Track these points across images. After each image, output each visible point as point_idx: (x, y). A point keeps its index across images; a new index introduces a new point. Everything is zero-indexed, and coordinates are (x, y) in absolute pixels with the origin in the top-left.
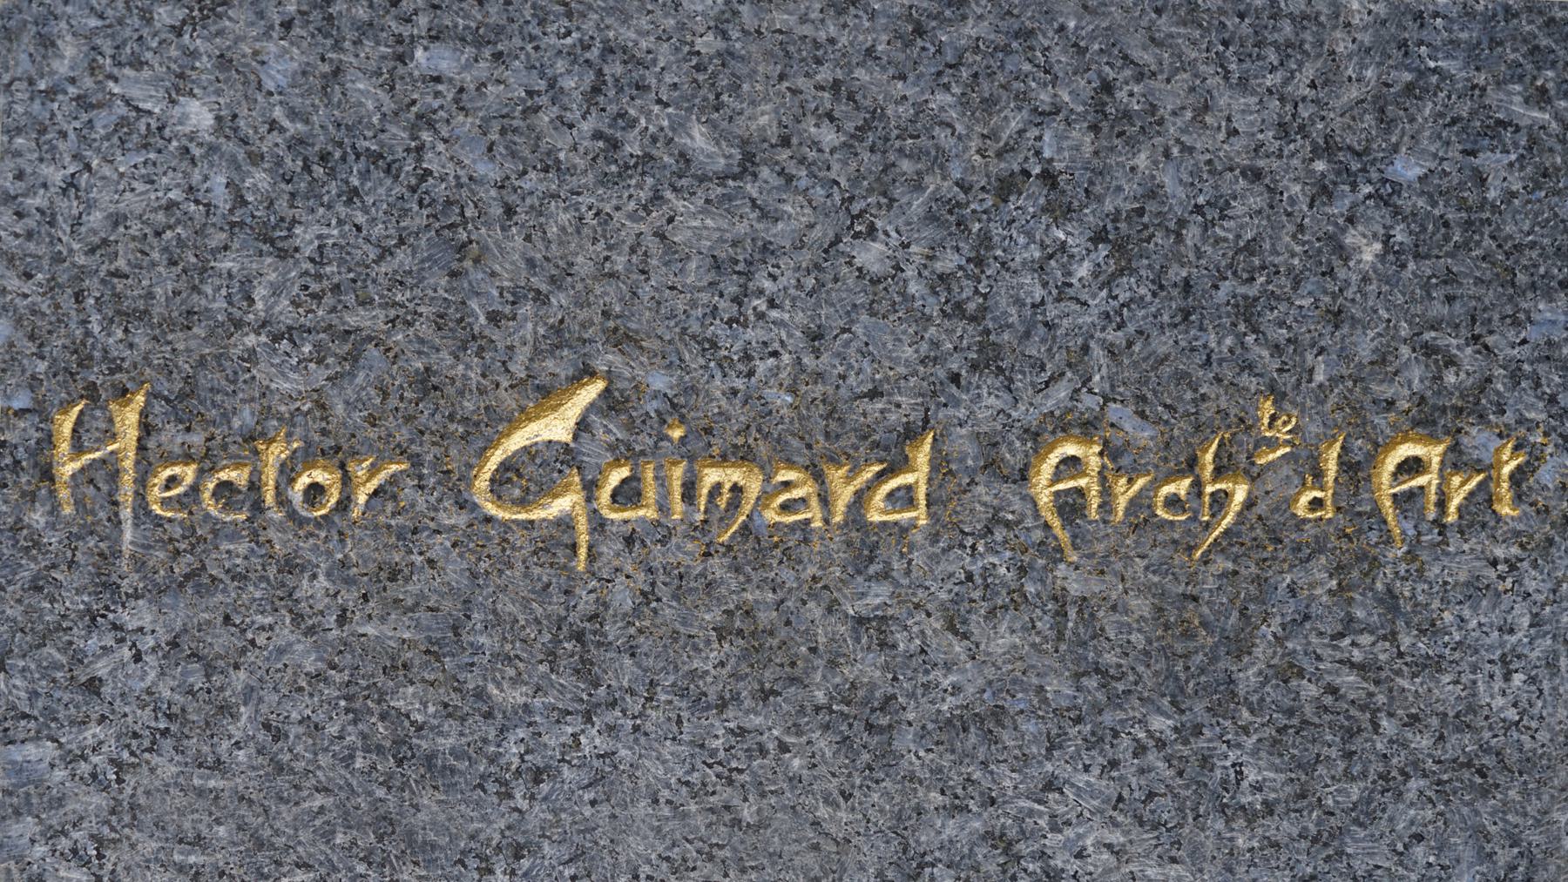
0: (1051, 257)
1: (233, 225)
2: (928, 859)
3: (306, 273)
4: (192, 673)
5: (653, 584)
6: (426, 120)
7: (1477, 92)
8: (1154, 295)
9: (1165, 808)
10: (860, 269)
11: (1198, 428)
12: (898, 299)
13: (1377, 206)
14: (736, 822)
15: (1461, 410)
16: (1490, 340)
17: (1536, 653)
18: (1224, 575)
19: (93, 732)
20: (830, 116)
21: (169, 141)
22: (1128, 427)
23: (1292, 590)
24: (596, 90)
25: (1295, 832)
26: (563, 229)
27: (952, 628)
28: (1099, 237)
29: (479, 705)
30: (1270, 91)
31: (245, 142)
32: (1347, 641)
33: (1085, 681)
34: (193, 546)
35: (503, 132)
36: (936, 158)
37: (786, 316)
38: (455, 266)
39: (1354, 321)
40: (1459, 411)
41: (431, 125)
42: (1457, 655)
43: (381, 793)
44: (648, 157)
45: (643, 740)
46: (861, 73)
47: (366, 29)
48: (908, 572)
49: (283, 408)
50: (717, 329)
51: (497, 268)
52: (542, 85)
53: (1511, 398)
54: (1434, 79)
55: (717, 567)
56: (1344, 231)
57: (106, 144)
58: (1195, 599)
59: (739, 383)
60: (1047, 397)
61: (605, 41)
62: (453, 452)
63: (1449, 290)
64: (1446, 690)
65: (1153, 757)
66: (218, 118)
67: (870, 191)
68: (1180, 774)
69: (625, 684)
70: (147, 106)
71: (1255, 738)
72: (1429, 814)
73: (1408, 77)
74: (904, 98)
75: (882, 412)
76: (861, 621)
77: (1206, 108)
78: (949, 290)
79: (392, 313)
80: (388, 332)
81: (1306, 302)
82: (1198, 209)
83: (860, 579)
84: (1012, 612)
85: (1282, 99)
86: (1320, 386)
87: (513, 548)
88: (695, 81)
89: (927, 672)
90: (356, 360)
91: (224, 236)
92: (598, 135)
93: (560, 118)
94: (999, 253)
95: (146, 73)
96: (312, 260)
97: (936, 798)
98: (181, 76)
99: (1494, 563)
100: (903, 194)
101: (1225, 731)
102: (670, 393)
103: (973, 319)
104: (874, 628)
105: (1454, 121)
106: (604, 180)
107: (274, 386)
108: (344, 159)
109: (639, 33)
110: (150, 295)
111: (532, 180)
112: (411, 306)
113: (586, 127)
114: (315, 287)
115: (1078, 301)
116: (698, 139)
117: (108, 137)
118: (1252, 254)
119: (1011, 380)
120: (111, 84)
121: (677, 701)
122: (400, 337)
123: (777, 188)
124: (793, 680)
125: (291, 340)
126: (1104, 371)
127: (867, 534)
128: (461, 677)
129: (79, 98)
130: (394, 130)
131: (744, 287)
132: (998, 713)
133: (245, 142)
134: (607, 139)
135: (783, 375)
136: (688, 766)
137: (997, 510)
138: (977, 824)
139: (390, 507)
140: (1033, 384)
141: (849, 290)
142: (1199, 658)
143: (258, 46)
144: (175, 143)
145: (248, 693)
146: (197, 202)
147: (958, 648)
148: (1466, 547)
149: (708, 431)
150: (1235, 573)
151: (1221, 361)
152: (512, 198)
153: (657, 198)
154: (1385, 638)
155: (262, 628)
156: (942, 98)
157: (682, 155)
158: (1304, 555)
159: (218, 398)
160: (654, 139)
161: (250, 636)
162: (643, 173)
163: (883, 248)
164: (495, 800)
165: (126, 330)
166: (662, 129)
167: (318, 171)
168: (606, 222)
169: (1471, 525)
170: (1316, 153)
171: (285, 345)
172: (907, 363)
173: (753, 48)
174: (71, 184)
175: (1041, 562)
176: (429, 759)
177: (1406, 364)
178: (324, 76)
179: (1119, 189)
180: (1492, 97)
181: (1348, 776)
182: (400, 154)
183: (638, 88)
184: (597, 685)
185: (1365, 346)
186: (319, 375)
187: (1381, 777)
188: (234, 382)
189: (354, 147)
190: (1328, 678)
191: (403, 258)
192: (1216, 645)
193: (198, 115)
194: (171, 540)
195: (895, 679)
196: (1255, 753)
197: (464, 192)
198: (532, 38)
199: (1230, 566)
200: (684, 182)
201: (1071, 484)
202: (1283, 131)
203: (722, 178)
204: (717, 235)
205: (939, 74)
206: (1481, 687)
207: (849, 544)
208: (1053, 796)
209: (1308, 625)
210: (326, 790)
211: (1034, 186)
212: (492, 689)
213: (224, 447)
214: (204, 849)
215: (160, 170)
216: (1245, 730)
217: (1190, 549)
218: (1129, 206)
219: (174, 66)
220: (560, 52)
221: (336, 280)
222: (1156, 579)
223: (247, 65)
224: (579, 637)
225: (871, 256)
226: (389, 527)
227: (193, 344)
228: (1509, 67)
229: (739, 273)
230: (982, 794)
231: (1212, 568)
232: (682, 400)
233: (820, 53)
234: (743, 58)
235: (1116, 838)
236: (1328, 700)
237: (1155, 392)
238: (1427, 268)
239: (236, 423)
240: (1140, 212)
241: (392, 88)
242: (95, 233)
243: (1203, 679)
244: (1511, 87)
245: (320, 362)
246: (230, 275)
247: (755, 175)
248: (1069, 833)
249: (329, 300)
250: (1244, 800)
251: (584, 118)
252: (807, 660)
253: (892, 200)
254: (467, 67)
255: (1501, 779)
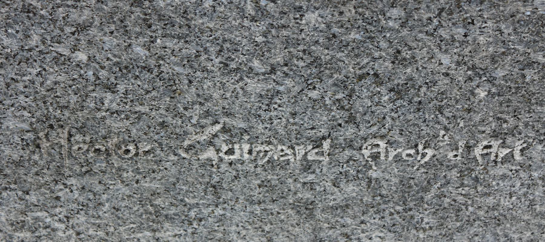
0: (375, 95)
1: (96, 85)
2: (323, 239)
3: (122, 97)
4: (89, 195)
5: (238, 174)
6: (161, 58)
7: (527, 54)
8: (409, 104)
9: (398, 229)
10: (310, 98)
11: (419, 137)
12: (322, 105)
13: (488, 83)
14: (263, 231)
15: (507, 134)
16: (519, 116)
17: (521, 192)
18: (424, 173)
19: (58, 210)
20: (302, 59)
21: (72, 63)
22: (396, 137)
23: (445, 177)
24: (220, 51)
25: (438, 234)
26: (209, 87)
27: (334, 185)
28: (391, 90)
29: (182, 203)
30: (455, 54)
31: (98, 63)
32: (461, 189)
33: (376, 198)
34: (88, 165)
35: (188, 61)
36: (338, 70)
37: (284, 109)
38: (173, 96)
39: (475, 111)
40: (506, 134)
41: (163, 59)
42: (495, 192)
43: (151, 224)
44: (238, 69)
45: (234, 211)
46: (313, 47)
47: (139, 34)
48: (321, 172)
49: (116, 131)
50: (261, 112)
51: (187, 96)
52: (202, 49)
53: (524, 131)
54: (513, 51)
55: (259, 170)
56: (475, 89)
57: (50, 63)
58: (413, 178)
59: (268, 126)
60: (370, 130)
61: (224, 38)
62: (172, 142)
63: (508, 104)
64: (491, 201)
65: (396, 216)
66: (89, 57)
67: (315, 78)
68: (404, 220)
69: (229, 198)
70: (64, 53)
71: (428, 212)
72: (481, 229)
73: (503, 50)
74: (328, 54)
75: (315, 133)
76: (305, 183)
77: (432, 58)
78: (340, 103)
79: (151, 107)
80: (150, 112)
81: (459, 107)
82: (427, 83)
83: (305, 173)
84: (354, 181)
85: (459, 55)
86: (461, 127)
87: (193, 165)
88: (255, 49)
89: (325, 196)
90: (139, 119)
91: (93, 87)
92: (221, 63)
93: (208, 58)
94: (357, 94)
95: (63, 45)
96: (124, 94)
97: (326, 225)
98: (75, 46)
99: (511, 171)
100: (326, 79)
101: (419, 210)
102: (245, 128)
103: (347, 110)
104: (311, 186)
105: (517, 62)
106: (223, 74)
107: (112, 125)
108: (133, 68)
109: (236, 36)
110: (69, 102)
111: (199, 74)
112: (157, 106)
113: (217, 61)
114: (125, 100)
115: (383, 106)
116: (256, 64)
117: (51, 62)
118: (443, 94)
119: (359, 126)
120: (51, 48)
121: (245, 202)
122: (154, 113)
123: (283, 77)
124: (282, 197)
125: (117, 114)
126: (390, 123)
127: (308, 163)
128: (176, 196)
129: (40, 51)
130: (150, 60)
131: (271, 102)
132: (347, 206)
133: (98, 63)
134: (224, 64)
135: (282, 124)
136: (248, 217)
137: (351, 157)
138: (339, 232)
139: (152, 155)
140: (365, 126)
141: (306, 103)
142: (412, 193)
143: (101, 38)
144: (74, 63)
145: (108, 200)
146: (83, 79)
147: (336, 189)
148: (503, 167)
149: (257, 137)
150: (427, 172)
151: (429, 121)
152: (192, 79)
153: (241, 79)
154: (473, 188)
155: (112, 184)
156: (340, 54)
157: (250, 68)
158: (450, 168)
159: (94, 128)
160: (241, 64)
161: (108, 186)
162: (237, 73)
163: (318, 92)
164: (187, 226)
165: (61, 111)
166: (243, 61)
167: (125, 71)
168: (224, 85)
169: (506, 161)
170: (469, 69)
171: (115, 115)
172: (324, 121)
173: (275, 41)
174: (39, 74)
175: (364, 169)
176: (166, 216)
177: (491, 122)
178: (125, 46)
179: (400, 78)
180: (532, 55)
181: (457, 220)
182: (153, 67)
183: (235, 50)
184: (219, 198)
185: (477, 118)
186: (128, 123)
187: (467, 221)
188: (99, 124)
189: (136, 65)
190: (453, 198)
191: (154, 93)
192: (419, 190)
193: (82, 56)
194: (80, 163)
195: (315, 197)
196: (428, 215)
197: (175, 77)
198: (198, 37)
199: (426, 171)
200: (251, 75)
201: (376, 150)
202: (458, 63)
203: (264, 74)
204: (261, 89)
205: (341, 48)
206: (502, 200)
207: (302, 165)
208: (363, 225)
209: (449, 185)
210: (134, 223)
211: (371, 77)
212: (186, 199)
213: (97, 140)
214: (101, 219)
215: (70, 70)
216: (426, 210)
217: (413, 167)
218: (402, 82)
219: (72, 43)
220: (208, 41)
221: (132, 99)
222: (401, 174)
223: (98, 43)
224: (214, 187)
225: (314, 94)
226: (152, 160)
227: (84, 114)
228: (539, 48)
229: (269, 98)
230: (341, 224)
231: (419, 171)
232: (248, 130)
233: (299, 42)
234: (272, 43)
235: (382, 235)
236: (453, 203)
237: (406, 129)
238: (501, 99)
239: (100, 134)
240: (407, 84)
241: (149, 50)
242: (48, 86)
243: (414, 197)
244: (539, 53)
245: (127, 119)
246: (95, 97)
247: (275, 74)
248: (367, 234)
249: (129, 103)
250: (423, 226)
251: (216, 58)
252: (287, 192)
253: (322, 80)
254: (176, 44)
255: (505, 222)
